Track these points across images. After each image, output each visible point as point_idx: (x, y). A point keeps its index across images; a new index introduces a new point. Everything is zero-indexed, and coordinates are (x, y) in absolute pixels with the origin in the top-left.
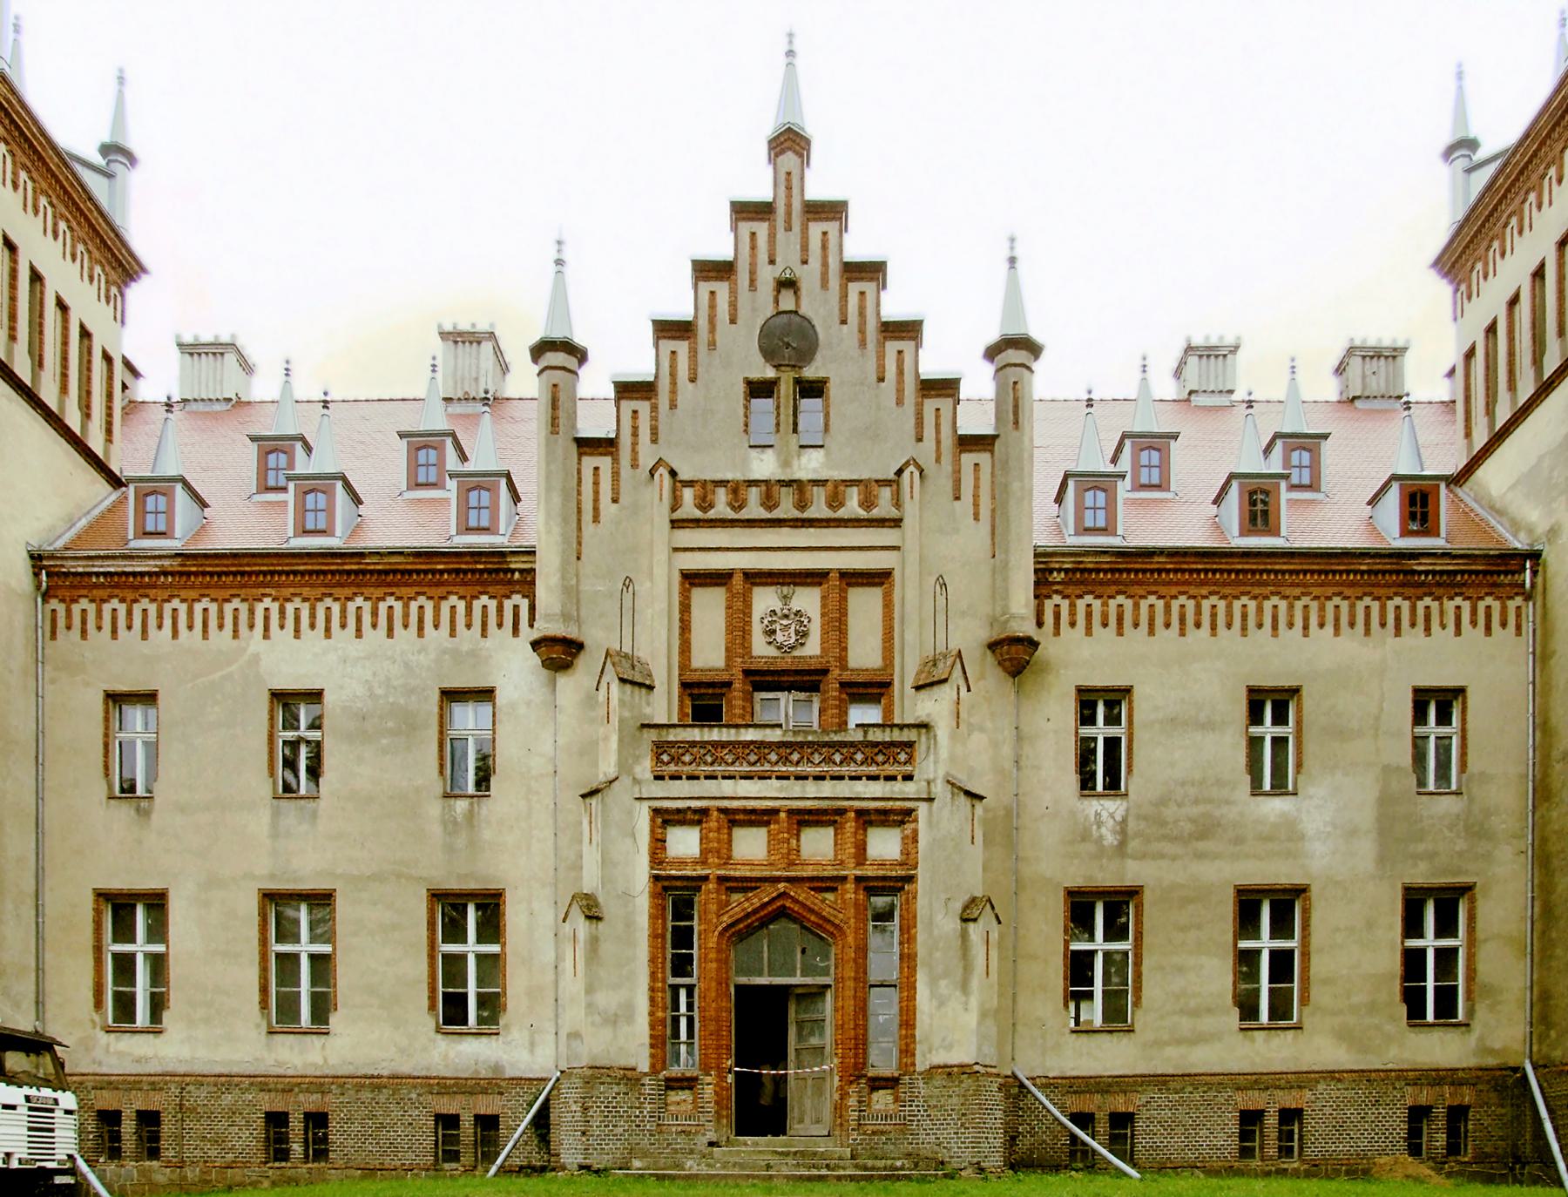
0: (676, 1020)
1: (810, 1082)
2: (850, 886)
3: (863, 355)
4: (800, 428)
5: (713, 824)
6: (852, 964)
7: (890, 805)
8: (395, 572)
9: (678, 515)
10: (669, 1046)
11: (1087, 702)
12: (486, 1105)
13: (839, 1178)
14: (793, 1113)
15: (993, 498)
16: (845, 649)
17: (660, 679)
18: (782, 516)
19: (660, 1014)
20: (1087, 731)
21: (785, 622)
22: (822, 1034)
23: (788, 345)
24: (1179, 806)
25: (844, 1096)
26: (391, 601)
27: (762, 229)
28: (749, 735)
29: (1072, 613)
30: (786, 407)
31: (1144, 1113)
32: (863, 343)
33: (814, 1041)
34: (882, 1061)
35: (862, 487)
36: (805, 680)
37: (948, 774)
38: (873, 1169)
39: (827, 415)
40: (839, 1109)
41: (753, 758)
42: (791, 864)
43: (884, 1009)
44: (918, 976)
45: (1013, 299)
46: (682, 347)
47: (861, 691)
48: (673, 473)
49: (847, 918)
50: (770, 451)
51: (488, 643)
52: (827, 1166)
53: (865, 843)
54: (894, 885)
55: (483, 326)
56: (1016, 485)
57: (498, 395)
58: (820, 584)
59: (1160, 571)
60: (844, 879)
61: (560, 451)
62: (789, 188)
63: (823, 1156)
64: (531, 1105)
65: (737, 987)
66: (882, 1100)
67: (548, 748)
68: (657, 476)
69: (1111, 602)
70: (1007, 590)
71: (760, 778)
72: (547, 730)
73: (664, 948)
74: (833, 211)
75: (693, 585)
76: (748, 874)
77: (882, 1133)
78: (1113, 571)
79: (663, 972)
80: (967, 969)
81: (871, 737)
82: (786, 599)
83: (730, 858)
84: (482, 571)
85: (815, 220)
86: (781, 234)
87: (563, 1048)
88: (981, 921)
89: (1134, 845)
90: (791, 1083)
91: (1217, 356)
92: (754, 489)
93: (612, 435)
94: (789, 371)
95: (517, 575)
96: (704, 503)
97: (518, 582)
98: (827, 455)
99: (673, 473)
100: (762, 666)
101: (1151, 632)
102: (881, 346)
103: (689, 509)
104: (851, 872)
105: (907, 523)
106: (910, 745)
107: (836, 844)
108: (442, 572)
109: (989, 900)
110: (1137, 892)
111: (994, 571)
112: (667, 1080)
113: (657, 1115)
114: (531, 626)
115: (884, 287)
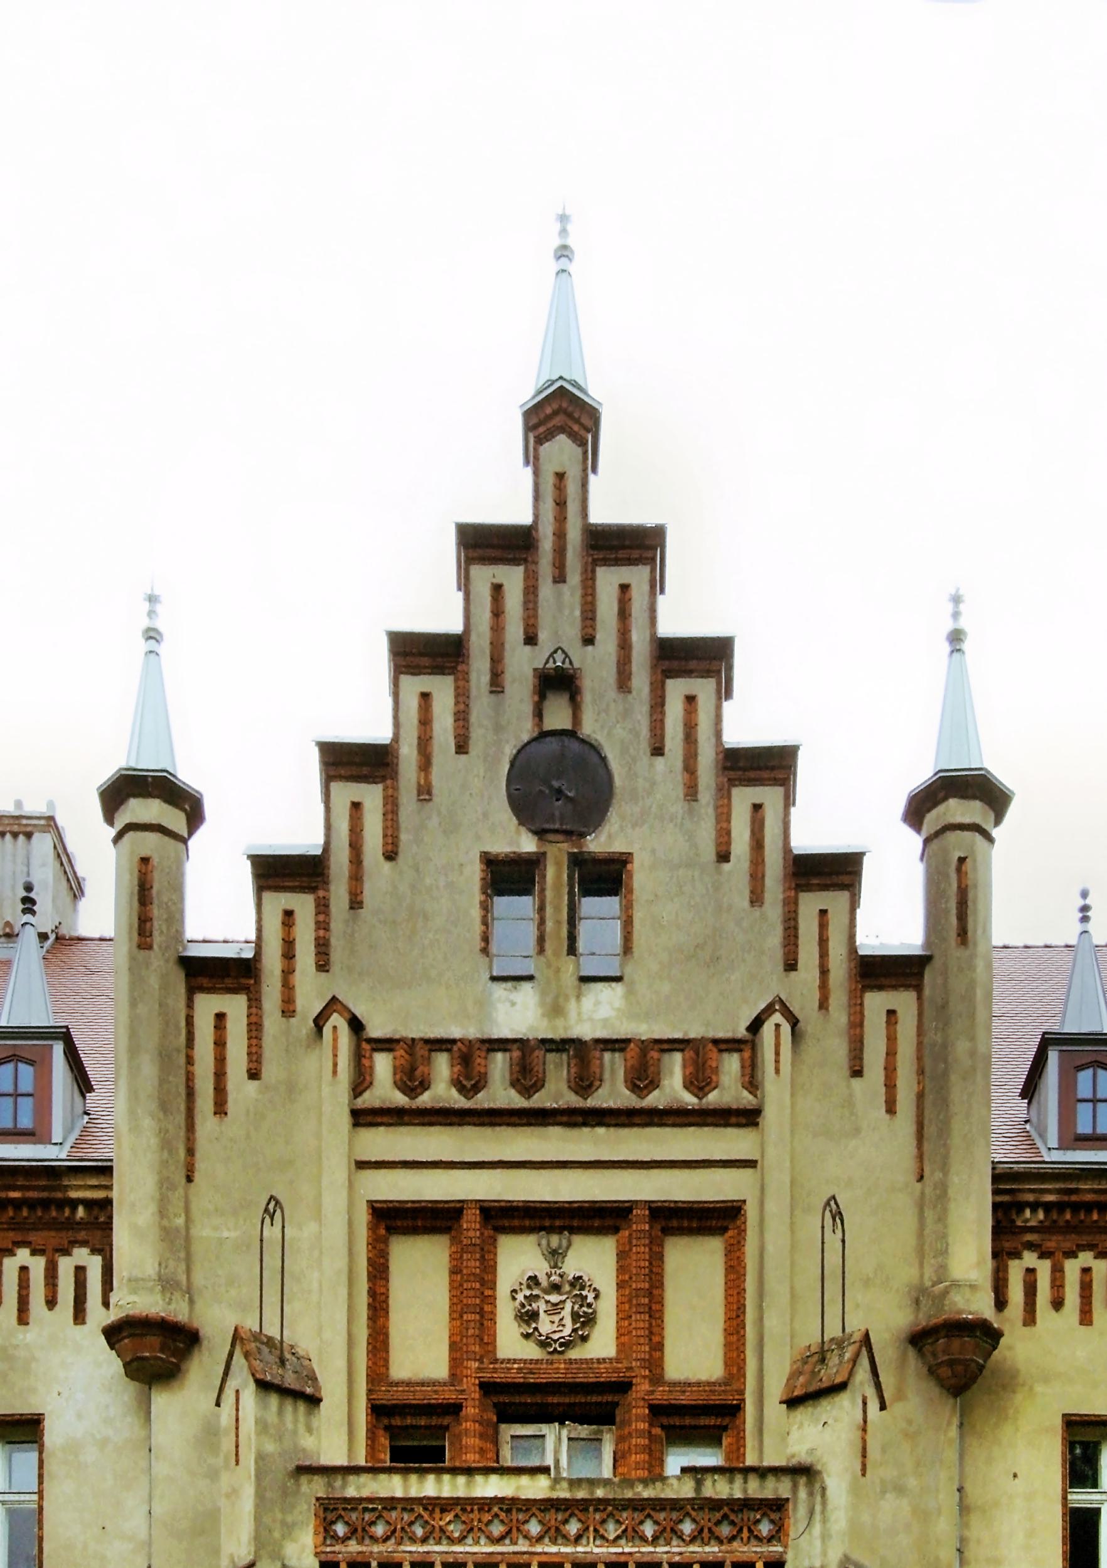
3: (691, 812)
4: (581, 945)
9: (368, 1100)
15: (921, 1072)
16: (659, 1347)
18: (549, 1104)
21: (554, 1298)
23: (559, 792)
27: (513, 578)
28: (491, 1487)
29: (1058, 1284)
30: (557, 909)
35: (690, 1054)
36: (588, 1402)
41: (497, 1529)
46: (372, 796)
47: (688, 1421)
48: (356, 1025)
50: (526, 986)
51: (29, 1335)
55: (34, 806)
56: (961, 1047)
57: (64, 931)
58: (615, 1230)
61: (154, 982)
62: (561, 503)
67: (136, 1524)
68: (327, 1030)
70: (943, 1236)
75: (392, 1230)
82: (555, 1256)
85: (606, 562)
86: (546, 589)
92: (499, 1056)
93: (249, 954)
95: (81, 1212)
97: (81, 1225)
98: (630, 992)
99: (356, 1025)
103: (384, 1088)
105: (771, 1116)
106: (777, 1506)
114: (106, 1304)
115: (729, 694)
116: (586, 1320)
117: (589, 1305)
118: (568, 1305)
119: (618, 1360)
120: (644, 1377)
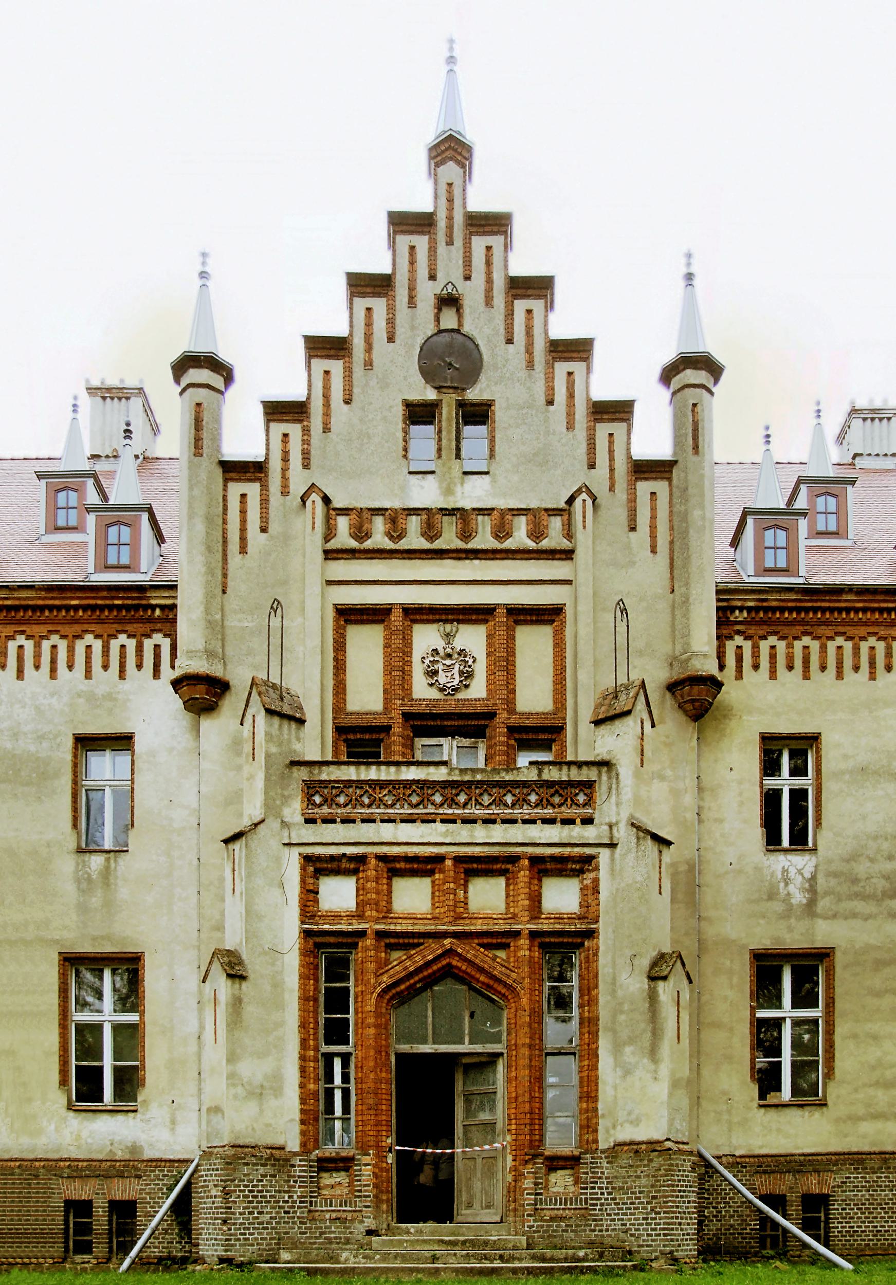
0: (330, 1094)
1: (479, 1161)
2: (524, 942)
5: (372, 873)
6: (526, 1029)
7: (567, 851)
8: (26, 608)
9: (333, 544)
10: (321, 1122)
11: (775, 750)
12: (122, 1190)
13: (515, 1271)
14: (461, 1196)
15: (672, 528)
16: (513, 691)
17: (312, 714)
19: (312, 1086)
20: (771, 783)
21: (448, 662)
22: (493, 1109)
24: (872, 860)
25: (518, 1177)
26: (21, 640)
27: (421, 242)
28: (411, 774)
29: (756, 655)
30: (449, 432)
31: (840, 1195)
32: (530, 365)
33: (484, 1116)
34: (560, 1137)
35: (530, 517)
36: (470, 724)
37: (632, 816)
38: (552, 1260)
39: (492, 440)
40: (513, 1191)
41: (415, 799)
42: (459, 917)
43: (560, 1076)
44: (601, 1042)
45: (690, 315)
48: (326, 500)
49: (520, 977)
50: (430, 477)
52: (501, 1257)
53: (540, 895)
54: (566, 946)
56: (697, 513)
57: (148, 454)
58: (486, 621)
59: (848, 610)
60: (516, 934)
61: (203, 476)
62: (450, 200)
63: (494, 1245)
64: (171, 1189)
65: (399, 1056)
66: (561, 1181)
68: (309, 503)
69: (796, 643)
71: (423, 821)
72: (192, 777)
73: (316, 1012)
74: (494, 224)
76: (410, 928)
77: (562, 1218)
78: (799, 610)
79: (316, 1039)
80: (656, 1034)
81: (546, 776)
82: (448, 637)
83: (389, 911)
84: (119, 608)
86: (442, 248)
87: (204, 1126)
88: (671, 980)
89: (823, 904)
90: (459, 1164)
91: (881, 419)
92: (414, 518)
94: (451, 398)
95: (158, 612)
96: (360, 533)
97: (159, 618)
98: (494, 481)
99: (326, 500)
100: (423, 709)
101: (840, 675)
102: (550, 366)
104: (525, 926)
106: (588, 786)
107: (507, 896)
108: (76, 608)
109: (680, 956)
110: (827, 955)
111: (673, 607)
112: (320, 1160)
113: (309, 1200)
114: (173, 667)
116: (468, 675)
117: (470, 666)
118: (457, 666)
119: (488, 700)
120: (504, 709)
